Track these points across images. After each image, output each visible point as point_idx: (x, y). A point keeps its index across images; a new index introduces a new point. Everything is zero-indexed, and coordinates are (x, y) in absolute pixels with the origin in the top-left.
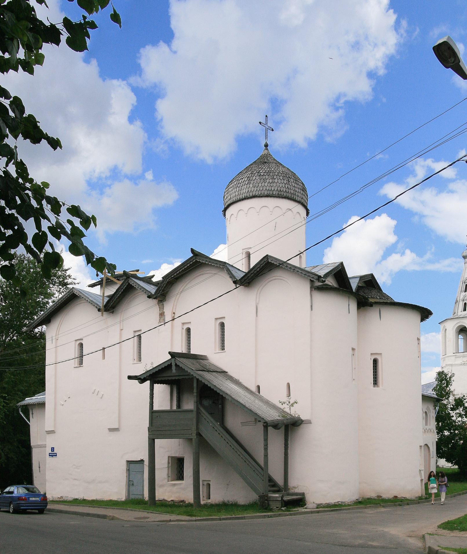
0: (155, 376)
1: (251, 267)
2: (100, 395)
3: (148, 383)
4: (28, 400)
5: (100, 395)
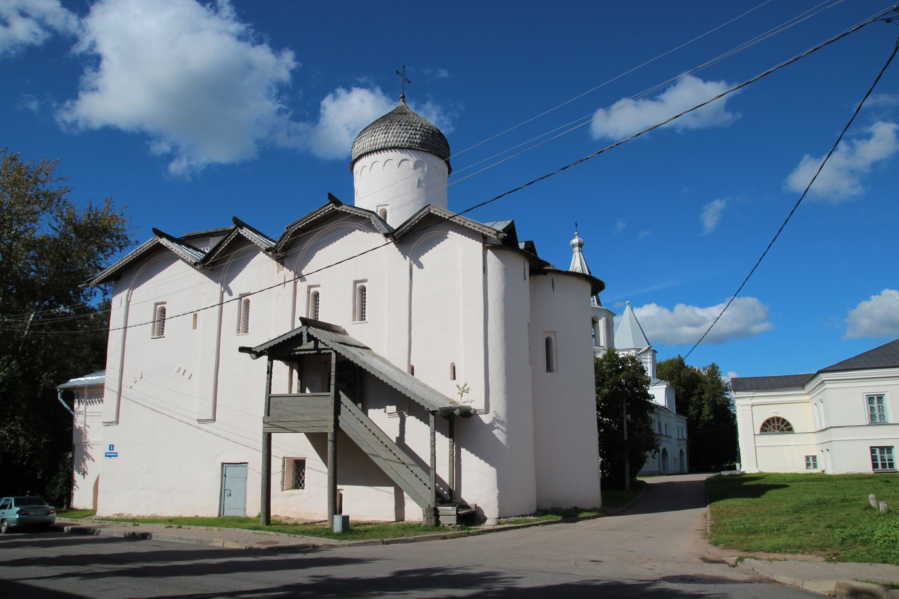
0: (279, 350)
1: (125, 292)
2: (187, 375)
3: (265, 358)
4: (73, 382)
5: (187, 375)
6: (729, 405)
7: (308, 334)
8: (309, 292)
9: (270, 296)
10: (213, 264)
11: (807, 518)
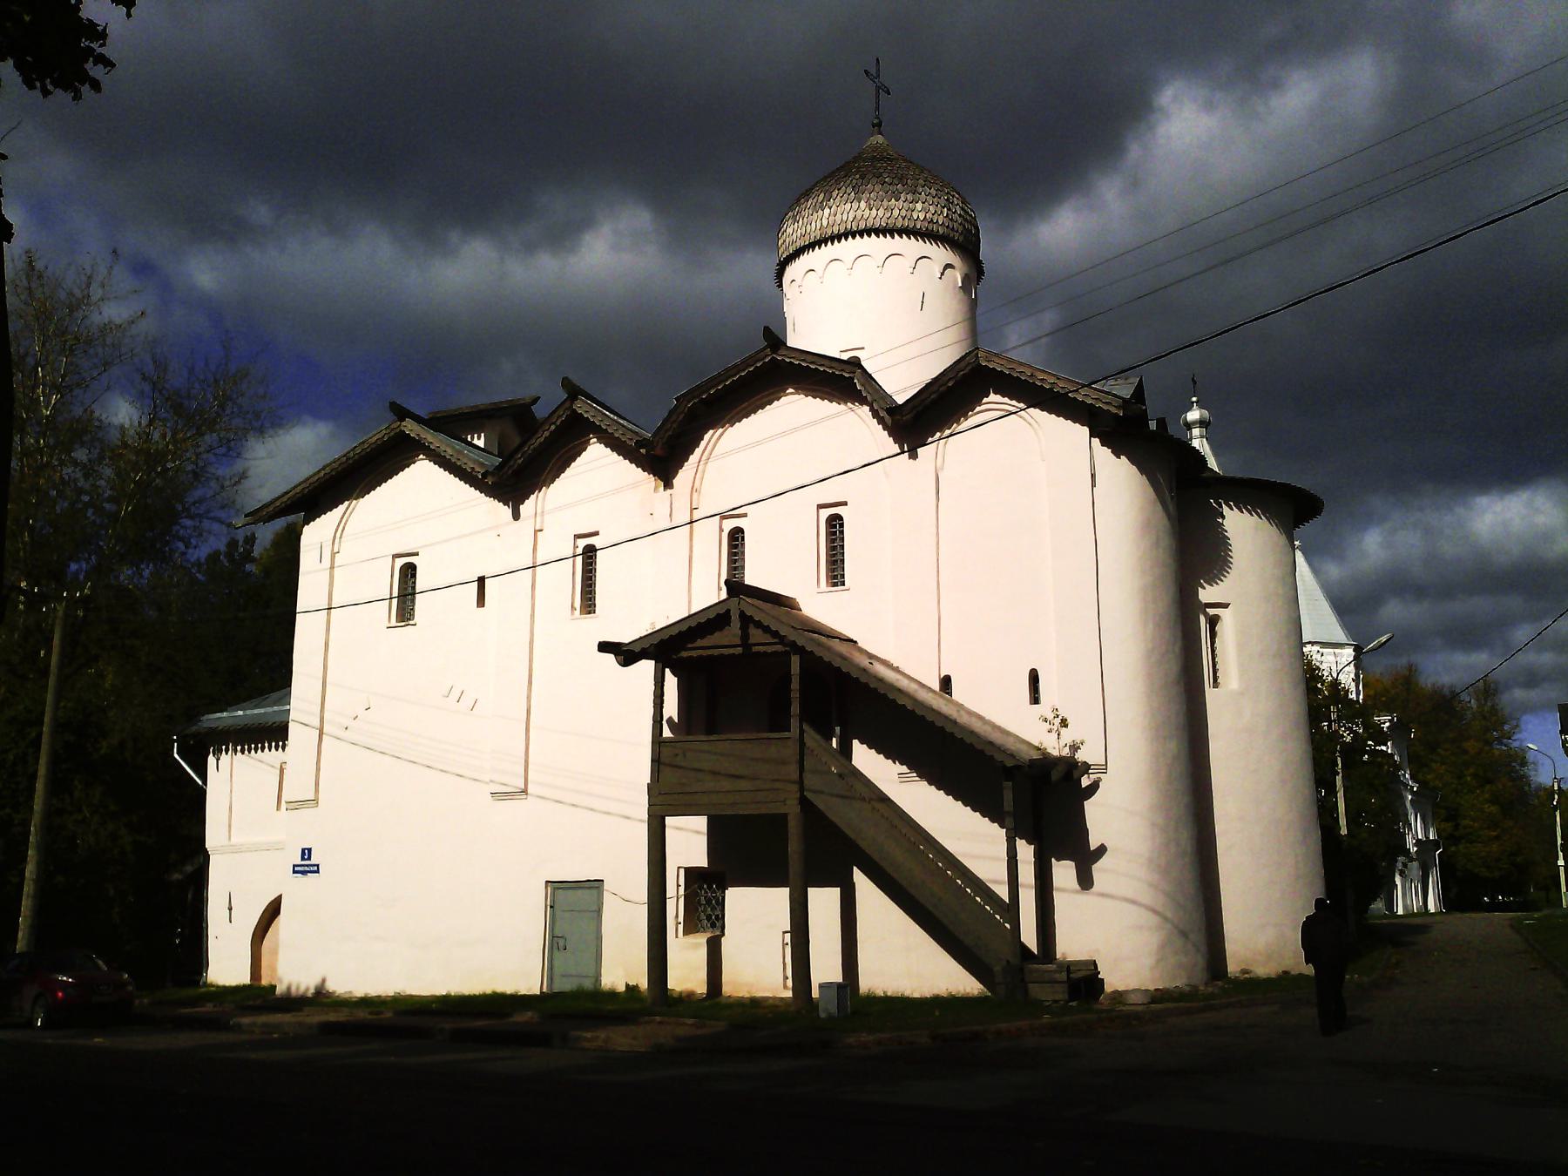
2: (467, 701)
3: (646, 667)
5: (467, 701)
6: (1524, 763)
7: (742, 615)
8: (721, 530)
9: (640, 539)
10: (518, 473)
11: (84, 278)
